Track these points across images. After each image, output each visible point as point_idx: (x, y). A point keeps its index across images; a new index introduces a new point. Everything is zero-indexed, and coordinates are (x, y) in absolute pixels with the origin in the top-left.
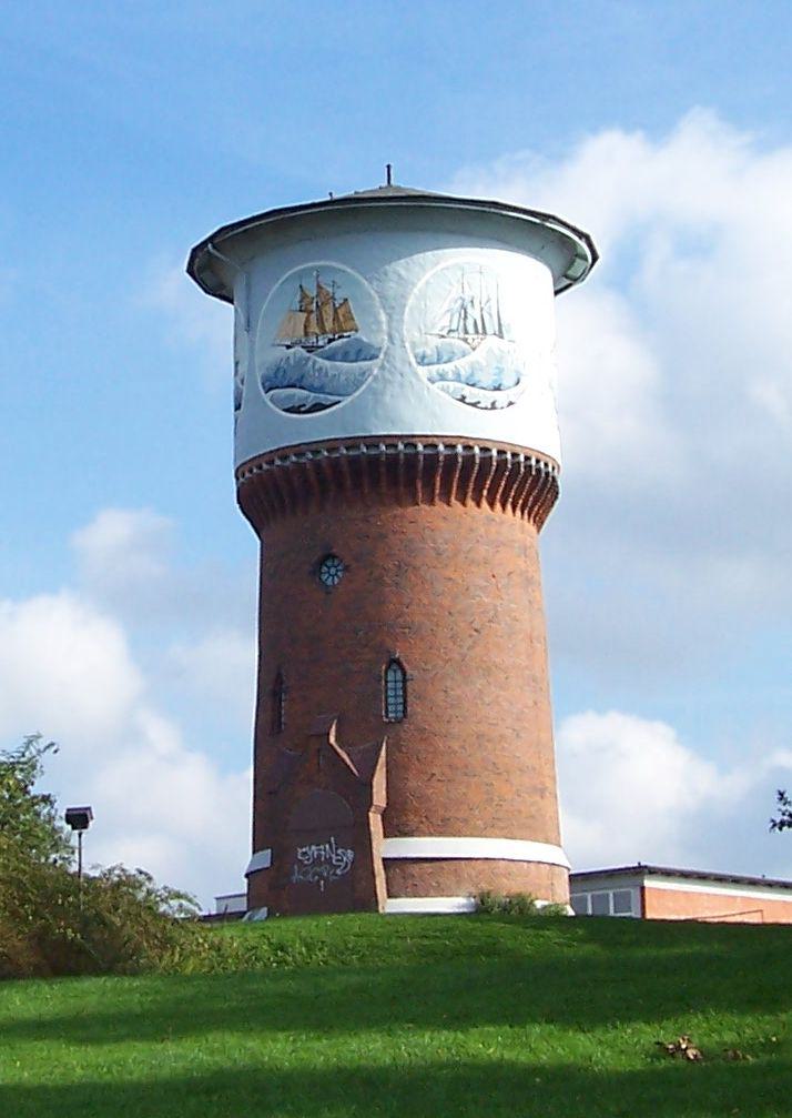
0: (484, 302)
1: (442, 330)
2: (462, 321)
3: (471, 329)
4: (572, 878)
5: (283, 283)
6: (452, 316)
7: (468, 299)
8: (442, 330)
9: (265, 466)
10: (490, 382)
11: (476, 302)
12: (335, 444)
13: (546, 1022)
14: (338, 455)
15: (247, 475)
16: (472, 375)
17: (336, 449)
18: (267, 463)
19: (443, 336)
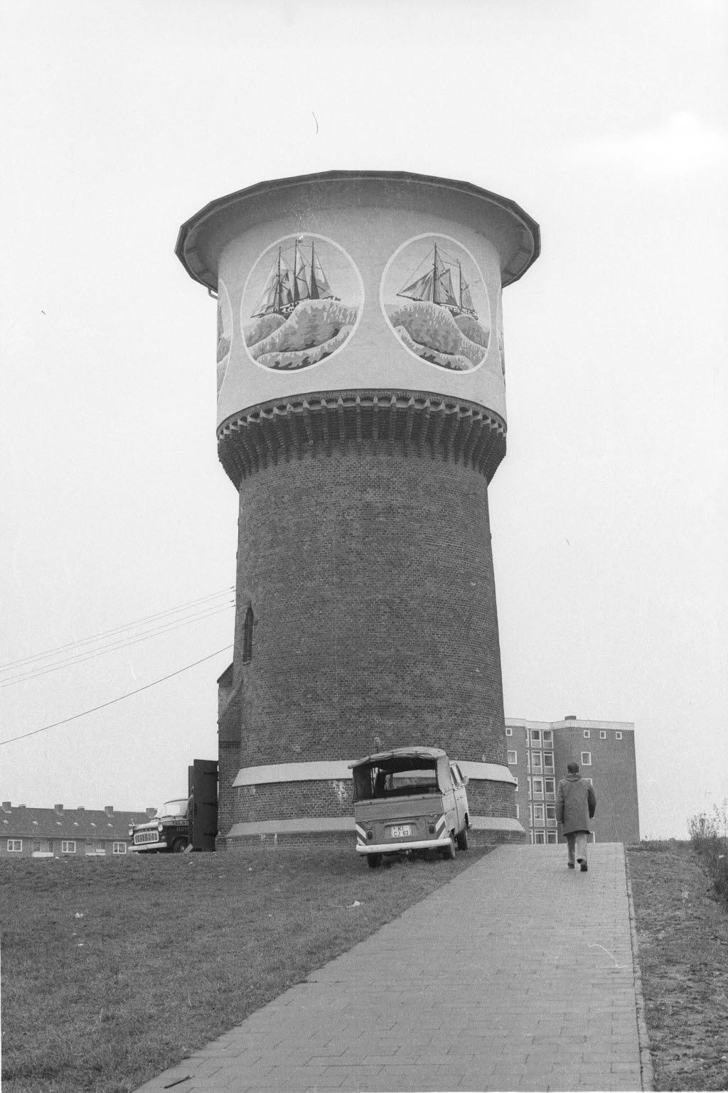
0: (298, 268)
1: (262, 310)
2: (278, 295)
3: (285, 300)
4: (470, 779)
5: (415, 242)
6: (270, 294)
7: (283, 273)
8: (262, 310)
9: (240, 423)
10: (302, 342)
11: (291, 277)
12: (300, 399)
13: (642, 955)
14: (302, 410)
15: (232, 427)
16: (285, 341)
17: (300, 404)
18: (241, 420)
19: (263, 315)
